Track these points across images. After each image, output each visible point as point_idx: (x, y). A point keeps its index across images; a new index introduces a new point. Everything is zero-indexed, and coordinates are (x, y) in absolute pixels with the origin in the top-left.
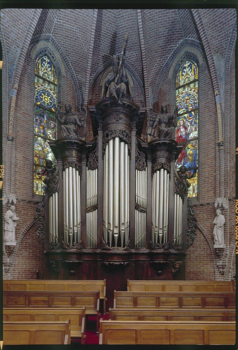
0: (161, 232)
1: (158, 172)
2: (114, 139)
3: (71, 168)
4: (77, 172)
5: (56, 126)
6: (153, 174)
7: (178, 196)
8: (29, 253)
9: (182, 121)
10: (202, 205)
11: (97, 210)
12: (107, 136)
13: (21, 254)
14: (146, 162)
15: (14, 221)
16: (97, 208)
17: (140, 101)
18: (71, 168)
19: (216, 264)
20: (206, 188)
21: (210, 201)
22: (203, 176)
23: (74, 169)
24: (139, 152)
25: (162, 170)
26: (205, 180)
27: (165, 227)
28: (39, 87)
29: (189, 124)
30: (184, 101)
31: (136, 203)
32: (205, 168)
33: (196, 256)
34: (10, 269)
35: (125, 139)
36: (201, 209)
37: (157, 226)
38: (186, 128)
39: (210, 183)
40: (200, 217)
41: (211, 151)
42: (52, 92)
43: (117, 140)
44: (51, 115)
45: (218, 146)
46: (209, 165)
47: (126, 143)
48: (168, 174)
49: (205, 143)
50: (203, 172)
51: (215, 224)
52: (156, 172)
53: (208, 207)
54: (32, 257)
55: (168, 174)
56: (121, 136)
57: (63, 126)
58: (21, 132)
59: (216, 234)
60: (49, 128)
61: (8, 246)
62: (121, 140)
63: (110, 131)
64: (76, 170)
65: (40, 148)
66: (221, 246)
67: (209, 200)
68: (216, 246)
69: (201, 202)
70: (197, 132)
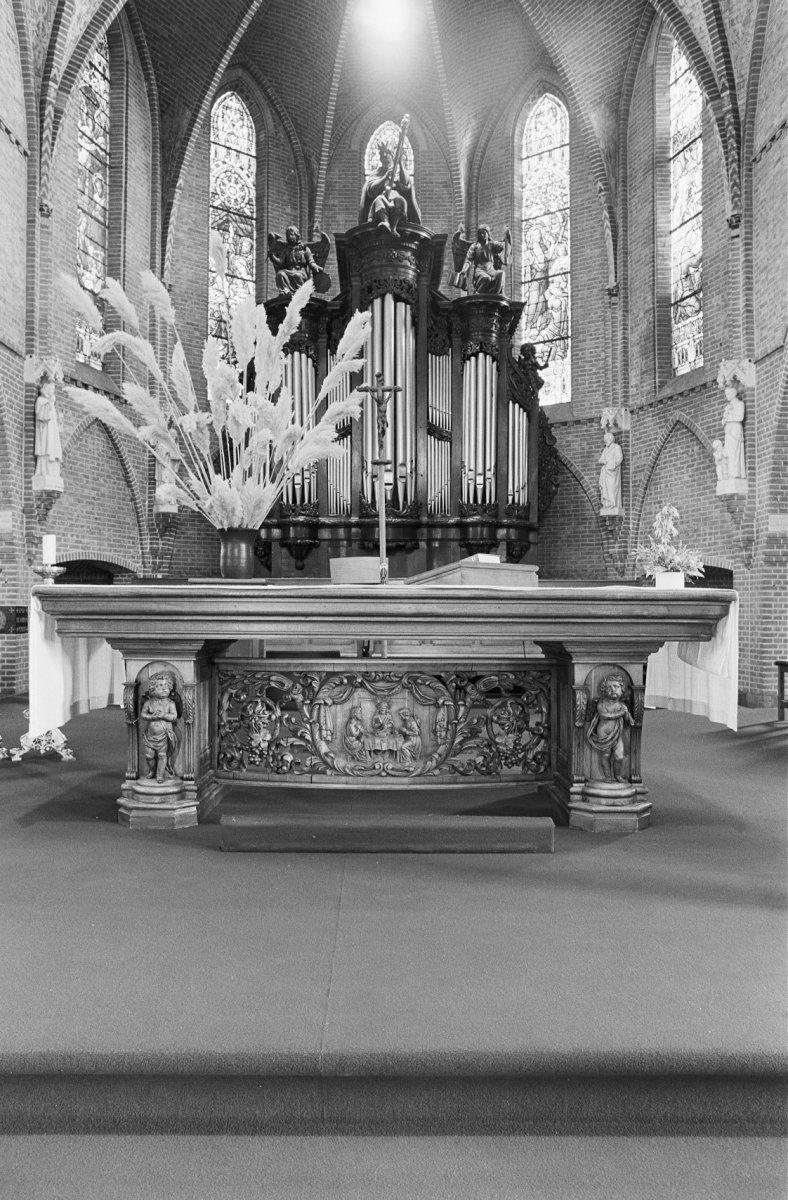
0: (480, 480)
1: (473, 359)
2: (383, 297)
3: (296, 354)
4: (310, 360)
5: (255, 247)
6: (464, 362)
7: (517, 406)
8: (198, 530)
9: (537, 232)
10: (578, 422)
11: (543, 656)
12: (370, 289)
13: (183, 533)
14: (450, 338)
15: (174, 461)
16: (351, 434)
17: (441, 183)
18: (296, 354)
19: (608, 553)
20: (587, 385)
21: (593, 413)
22: (581, 359)
23: (304, 356)
24: (434, 317)
25: (481, 355)
26: (584, 367)
27: (490, 470)
28: (218, 166)
29: (551, 239)
30: (540, 188)
31: (429, 423)
32: (584, 341)
33: (569, 537)
34: (162, 563)
35: (403, 295)
36: (577, 432)
37: (472, 467)
38: (545, 249)
39: (595, 374)
40: (574, 449)
41: (594, 304)
42: (243, 174)
43: (389, 298)
44: (242, 226)
45: (609, 294)
46: (591, 335)
47: (407, 302)
48: (495, 363)
49: (585, 286)
50: (581, 350)
51: (602, 465)
52: (469, 359)
53: (592, 426)
54: (204, 539)
55: (495, 363)
56: (398, 291)
57: (283, 273)
58: (185, 271)
59: (604, 487)
60: (239, 253)
61: (164, 514)
62: (397, 299)
63: (375, 281)
64: (308, 357)
65: (221, 299)
66: (615, 512)
67: (593, 411)
68: (603, 512)
69: (577, 415)
70: (567, 260)
